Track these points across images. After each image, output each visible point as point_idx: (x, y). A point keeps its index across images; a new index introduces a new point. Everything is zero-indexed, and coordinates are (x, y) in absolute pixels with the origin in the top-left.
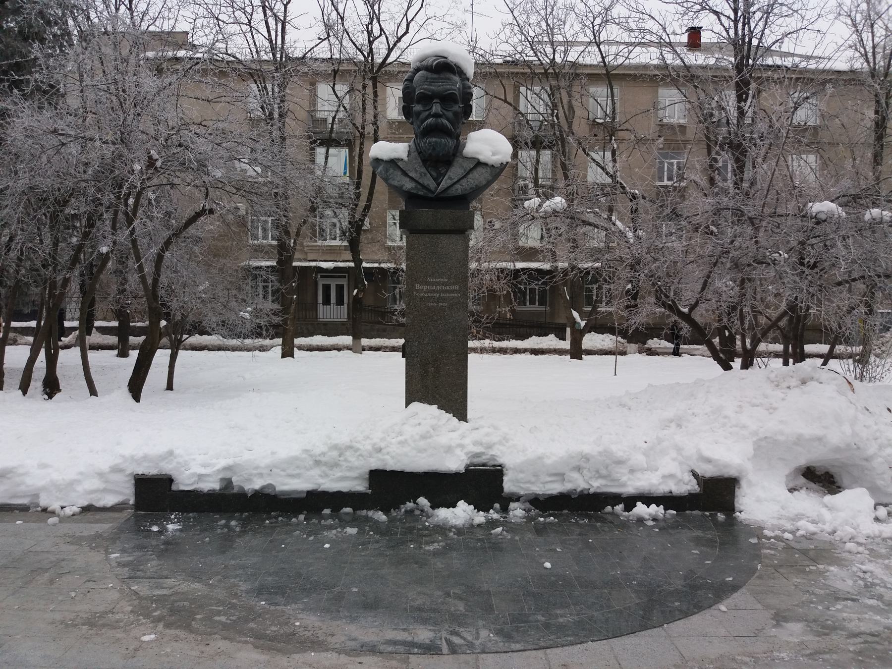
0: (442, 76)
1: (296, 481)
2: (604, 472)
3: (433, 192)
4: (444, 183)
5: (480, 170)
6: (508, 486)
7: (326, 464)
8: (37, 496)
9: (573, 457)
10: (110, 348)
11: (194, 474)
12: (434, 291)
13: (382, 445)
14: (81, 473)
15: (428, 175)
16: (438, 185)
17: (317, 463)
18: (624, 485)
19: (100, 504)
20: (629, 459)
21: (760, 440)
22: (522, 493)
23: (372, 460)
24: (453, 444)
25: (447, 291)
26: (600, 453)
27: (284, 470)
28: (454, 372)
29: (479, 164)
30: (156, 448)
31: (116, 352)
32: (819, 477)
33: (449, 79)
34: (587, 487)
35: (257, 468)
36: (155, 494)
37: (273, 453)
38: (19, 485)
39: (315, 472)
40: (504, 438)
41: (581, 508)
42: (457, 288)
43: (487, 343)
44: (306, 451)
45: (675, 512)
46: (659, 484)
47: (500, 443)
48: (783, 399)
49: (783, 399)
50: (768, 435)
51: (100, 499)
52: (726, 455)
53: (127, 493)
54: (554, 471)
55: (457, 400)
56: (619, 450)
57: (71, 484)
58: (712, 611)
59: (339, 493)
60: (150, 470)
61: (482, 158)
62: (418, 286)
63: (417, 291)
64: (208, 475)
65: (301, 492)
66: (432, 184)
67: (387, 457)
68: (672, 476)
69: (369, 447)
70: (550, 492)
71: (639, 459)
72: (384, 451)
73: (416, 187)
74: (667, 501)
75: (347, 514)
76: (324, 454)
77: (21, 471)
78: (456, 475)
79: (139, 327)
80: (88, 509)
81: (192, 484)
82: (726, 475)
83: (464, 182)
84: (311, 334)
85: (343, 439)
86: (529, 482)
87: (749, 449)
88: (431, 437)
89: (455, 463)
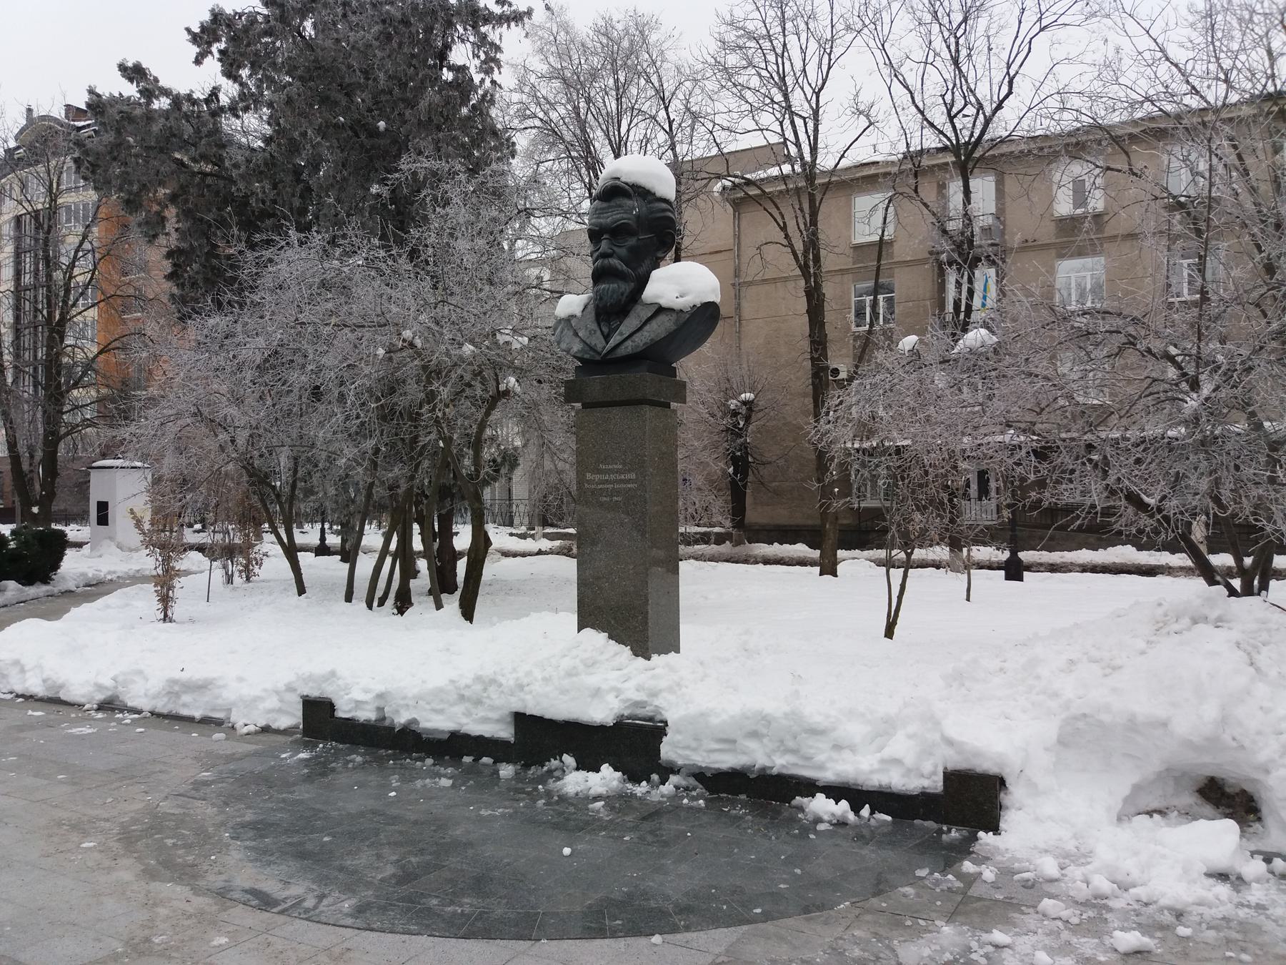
0: (612, 203)
1: (440, 717)
2: (791, 744)
3: (599, 354)
4: (612, 342)
5: (662, 318)
6: (668, 750)
7: (469, 699)
8: (230, 710)
9: (748, 718)
10: (812, 563)
11: (351, 700)
12: (607, 482)
13: (525, 681)
14: (265, 690)
15: (599, 332)
17: (462, 698)
18: (821, 767)
19: (274, 726)
20: (834, 729)
21: (1076, 718)
22: (680, 762)
23: (513, 699)
24: (604, 686)
25: (622, 481)
26: (786, 714)
27: (428, 703)
29: (660, 310)
30: (319, 666)
31: (817, 569)
32: (1231, 797)
34: (768, 764)
35: (404, 698)
36: (319, 716)
37: (424, 682)
38: (217, 698)
39: (459, 709)
40: (679, 685)
41: (766, 793)
42: (633, 476)
43: (1085, 556)
44: (452, 682)
45: (889, 818)
46: (872, 772)
47: (670, 690)
48: (1143, 653)
49: (1143, 653)
50: (1087, 711)
51: (275, 720)
52: (987, 734)
53: (291, 717)
54: (725, 737)
56: (815, 710)
57: (256, 699)
58: (642, 941)
59: (480, 739)
60: (315, 693)
61: (664, 302)
62: (589, 476)
63: (589, 482)
64: (366, 702)
65: (443, 732)
67: (528, 697)
68: (897, 762)
69: (512, 683)
70: (716, 766)
71: (854, 730)
72: (526, 689)
74: (882, 799)
75: (485, 765)
76: (467, 686)
77: (220, 683)
78: (602, 728)
79: (717, 534)
80: (266, 730)
81: (350, 711)
82: (979, 770)
83: (637, 338)
84: (1105, 544)
85: (488, 672)
86: (688, 747)
87: (1050, 729)
88: (577, 675)
89: (601, 712)
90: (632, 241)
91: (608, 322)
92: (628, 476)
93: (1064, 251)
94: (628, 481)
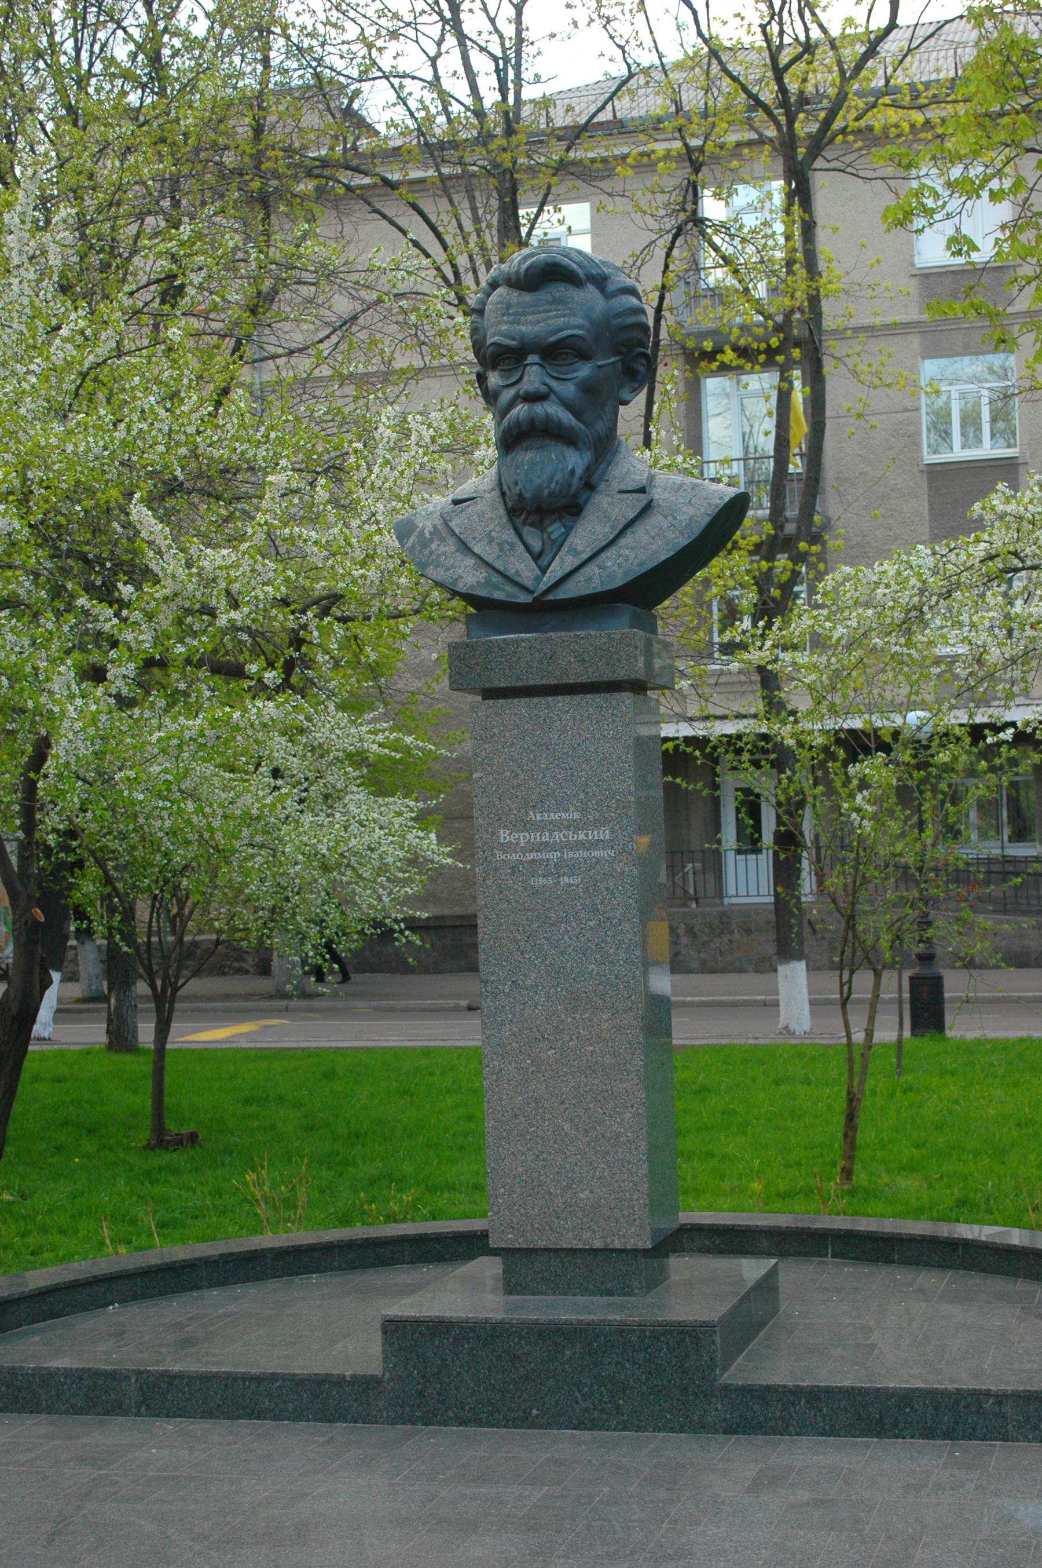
4: (556, 570)
12: (546, 846)
15: (521, 548)
16: (544, 571)
28: (608, 1059)
33: (561, 302)
42: (605, 834)
55: (618, 1136)
62: (504, 836)
63: (505, 847)
66: (523, 568)
73: (488, 583)
90: (584, 371)
91: (540, 526)
92: (594, 835)
93: (938, 337)
94: (595, 844)
